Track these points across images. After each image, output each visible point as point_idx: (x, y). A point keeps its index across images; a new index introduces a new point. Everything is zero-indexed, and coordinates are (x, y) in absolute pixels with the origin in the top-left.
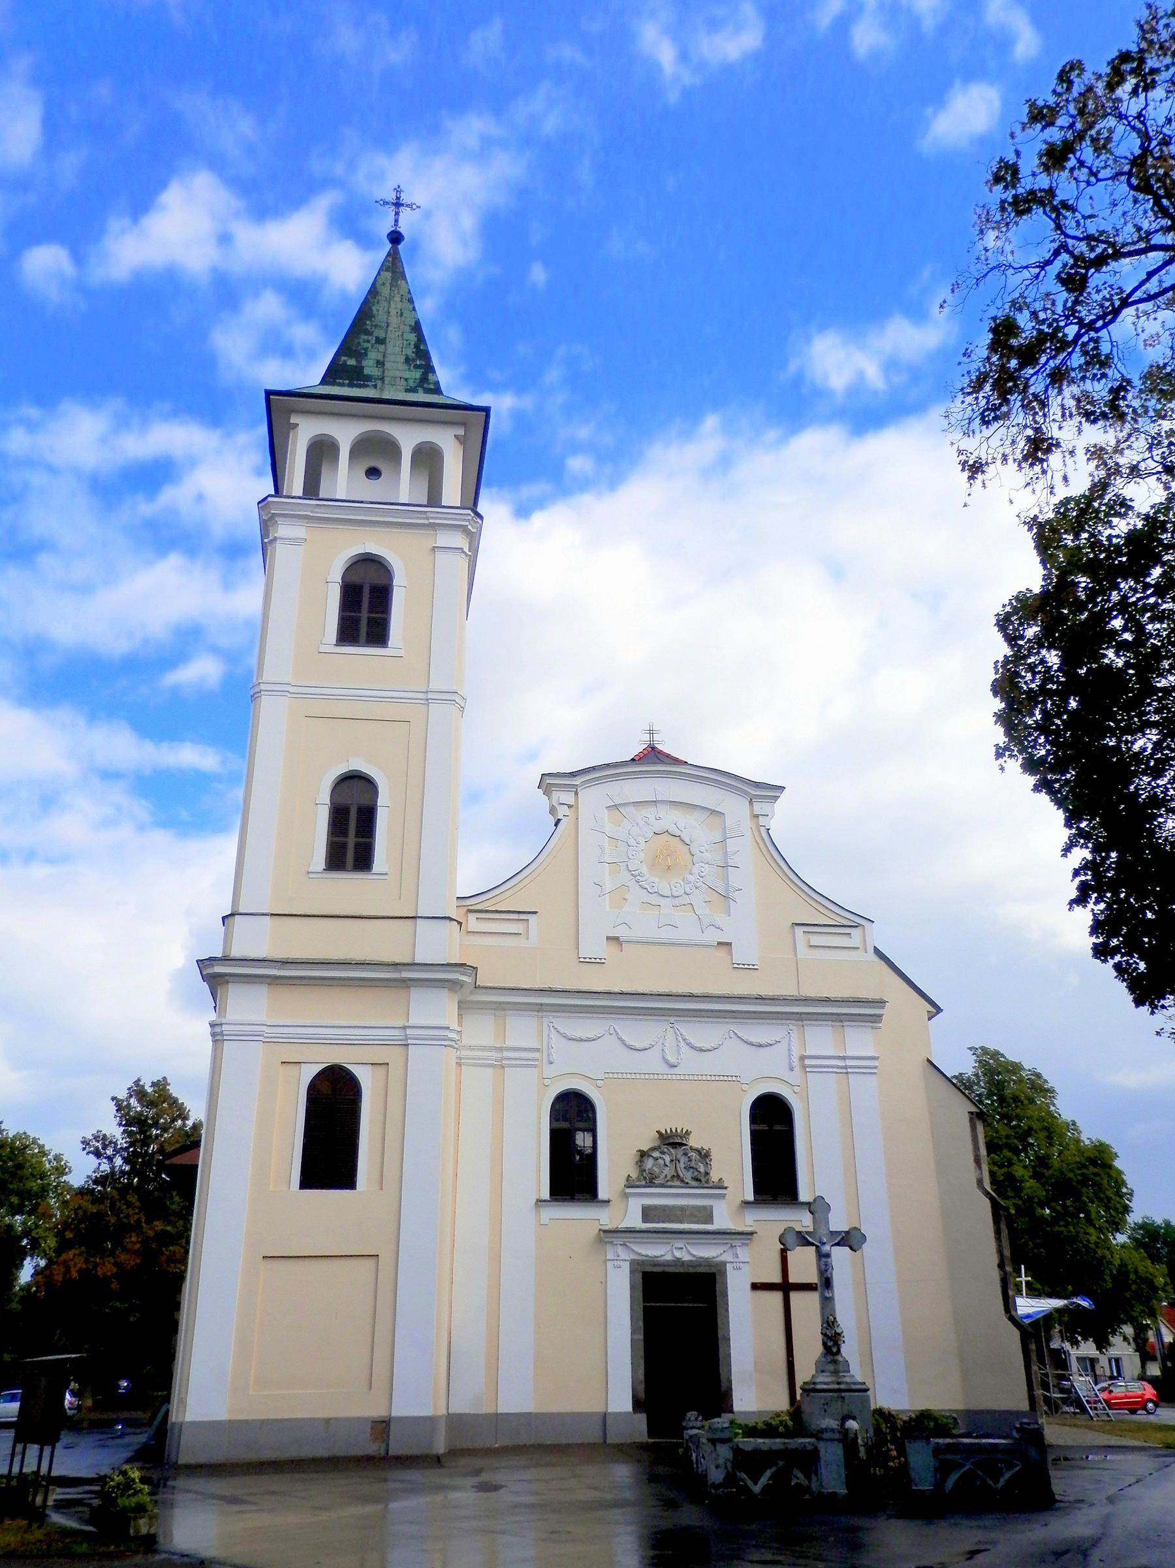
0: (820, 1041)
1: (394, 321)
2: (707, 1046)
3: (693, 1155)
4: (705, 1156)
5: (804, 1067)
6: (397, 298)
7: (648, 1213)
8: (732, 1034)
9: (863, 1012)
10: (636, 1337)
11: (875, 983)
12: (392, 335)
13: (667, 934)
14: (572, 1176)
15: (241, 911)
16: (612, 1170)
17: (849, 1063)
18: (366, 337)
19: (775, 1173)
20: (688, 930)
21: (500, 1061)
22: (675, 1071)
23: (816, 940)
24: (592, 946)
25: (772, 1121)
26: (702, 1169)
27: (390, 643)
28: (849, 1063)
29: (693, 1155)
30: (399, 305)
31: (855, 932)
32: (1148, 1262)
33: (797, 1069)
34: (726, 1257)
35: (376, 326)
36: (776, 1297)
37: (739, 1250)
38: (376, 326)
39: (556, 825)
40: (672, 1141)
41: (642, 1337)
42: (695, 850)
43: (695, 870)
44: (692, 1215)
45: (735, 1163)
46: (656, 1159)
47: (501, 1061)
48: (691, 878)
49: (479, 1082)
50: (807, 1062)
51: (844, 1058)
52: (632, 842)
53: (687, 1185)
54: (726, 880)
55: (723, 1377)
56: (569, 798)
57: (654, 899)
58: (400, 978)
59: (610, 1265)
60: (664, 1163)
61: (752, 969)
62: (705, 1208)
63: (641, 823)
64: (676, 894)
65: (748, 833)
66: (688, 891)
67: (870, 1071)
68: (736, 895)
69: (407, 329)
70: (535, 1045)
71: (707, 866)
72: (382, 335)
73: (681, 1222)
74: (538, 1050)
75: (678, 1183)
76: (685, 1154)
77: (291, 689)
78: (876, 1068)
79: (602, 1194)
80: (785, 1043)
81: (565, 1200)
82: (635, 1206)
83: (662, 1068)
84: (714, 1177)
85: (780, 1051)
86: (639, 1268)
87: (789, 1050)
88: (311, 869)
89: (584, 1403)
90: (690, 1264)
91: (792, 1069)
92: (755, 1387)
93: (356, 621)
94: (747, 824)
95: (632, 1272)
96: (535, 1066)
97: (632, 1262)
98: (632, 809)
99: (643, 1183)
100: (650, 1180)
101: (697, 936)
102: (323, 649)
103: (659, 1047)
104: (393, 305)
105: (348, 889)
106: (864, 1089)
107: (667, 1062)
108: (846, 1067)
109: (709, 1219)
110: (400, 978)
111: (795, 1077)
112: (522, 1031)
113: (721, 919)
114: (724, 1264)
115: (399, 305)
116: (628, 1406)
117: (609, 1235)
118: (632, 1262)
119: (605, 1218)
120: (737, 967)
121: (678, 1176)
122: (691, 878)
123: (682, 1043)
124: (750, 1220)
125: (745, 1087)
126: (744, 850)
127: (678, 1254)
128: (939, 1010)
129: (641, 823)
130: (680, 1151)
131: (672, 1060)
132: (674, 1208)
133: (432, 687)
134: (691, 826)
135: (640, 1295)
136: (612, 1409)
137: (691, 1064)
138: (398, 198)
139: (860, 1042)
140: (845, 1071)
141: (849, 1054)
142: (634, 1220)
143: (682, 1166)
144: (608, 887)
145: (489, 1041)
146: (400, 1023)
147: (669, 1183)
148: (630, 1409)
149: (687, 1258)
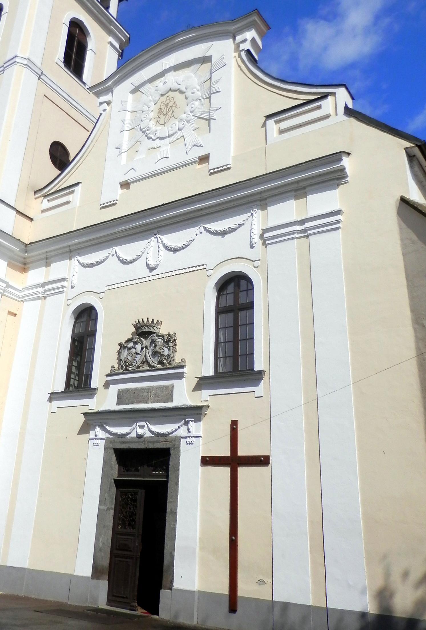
2: (179, 245)
4: (169, 340)
5: (264, 244)
7: (121, 397)
17: (308, 225)
22: (154, 272)
23: (285, 125)
26: (166, 352)
32: (153, 122)
34: (182, 432)
46: (130, 349)
52: (145, 108)
53: (153, 368)
62: (167, 387)
73: (147, 402)
76: (153, 342)
78: (338, 222)
79: (94, 384)
81: (420, 378)
84: (177, 359)
86: (111, 445)
90: (150, 440)
92: (193, 567)
95: (106, 449)
97: (107, 440)
98: (148, 86)
99: (121, 371)
106: (327, 247)
108: (305, 230)
117: (93, 420)
118: (107, 440)
119: (94, 404)
124: (204, 397)
125: (209, 273)
127: (140, 431)
132: (143, 389)
137: (168, 262)
147: (141, 369)
149: (148, 434)
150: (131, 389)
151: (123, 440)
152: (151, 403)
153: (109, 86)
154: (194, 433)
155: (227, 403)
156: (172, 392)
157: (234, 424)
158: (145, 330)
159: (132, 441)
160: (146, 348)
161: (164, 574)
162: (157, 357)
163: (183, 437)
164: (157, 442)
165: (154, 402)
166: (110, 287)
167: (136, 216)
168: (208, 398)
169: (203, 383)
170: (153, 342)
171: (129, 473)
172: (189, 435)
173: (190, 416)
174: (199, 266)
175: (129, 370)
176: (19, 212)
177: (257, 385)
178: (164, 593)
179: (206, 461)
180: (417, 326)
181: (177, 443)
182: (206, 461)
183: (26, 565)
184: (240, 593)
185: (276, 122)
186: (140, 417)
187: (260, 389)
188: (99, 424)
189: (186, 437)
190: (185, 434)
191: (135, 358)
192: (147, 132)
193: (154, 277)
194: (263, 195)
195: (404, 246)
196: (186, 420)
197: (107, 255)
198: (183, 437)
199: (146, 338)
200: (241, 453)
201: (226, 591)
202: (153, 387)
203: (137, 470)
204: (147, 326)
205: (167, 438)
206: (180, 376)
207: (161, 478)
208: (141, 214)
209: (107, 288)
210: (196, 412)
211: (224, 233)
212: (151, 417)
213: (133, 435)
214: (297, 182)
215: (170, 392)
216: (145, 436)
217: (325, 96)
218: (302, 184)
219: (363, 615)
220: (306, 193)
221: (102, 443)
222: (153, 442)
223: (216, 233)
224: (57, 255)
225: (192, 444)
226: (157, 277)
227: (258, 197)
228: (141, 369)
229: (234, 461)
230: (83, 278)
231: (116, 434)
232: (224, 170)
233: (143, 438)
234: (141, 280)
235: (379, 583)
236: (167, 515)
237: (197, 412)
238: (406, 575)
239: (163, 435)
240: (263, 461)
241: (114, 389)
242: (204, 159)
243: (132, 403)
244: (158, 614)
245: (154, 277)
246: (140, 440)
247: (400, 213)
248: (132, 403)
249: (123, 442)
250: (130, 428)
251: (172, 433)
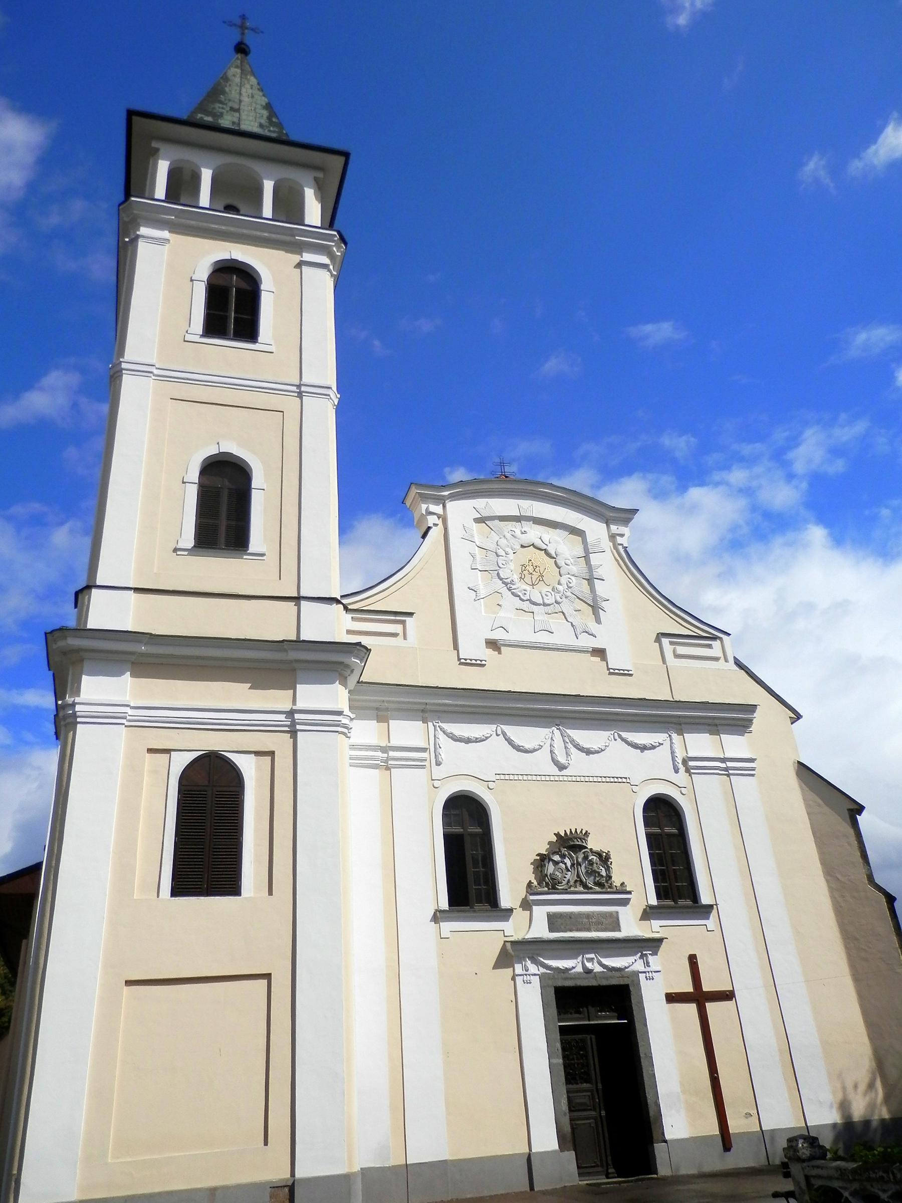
0: (700, 744)
1: (246, 100)
3: (594, 858)
5: (688, 770)
6: (248, 86)
7: (554, 922)
8: (617, 737)
9: (733, 719)
10: (554, 1061)
11: (741, 691)
12: (245, 107)
13: (543, 638)
14: (469, 880)
15: (98, 584)
16: (512, 875)
17: (730, 764)
18: (221, 106)
20: (562, 636)
21: (386, 760)
22: (564, 772)
23: (681, 650)
24: (472, 648)
25: (664, 821)
26: (604, 873)
27: (260, 339)
28: (730, 764)
29: (594, 858)
30: (250, 91)
31: (716, 644)
33: (682, 769)
34: (639, 966)
35: (230, 100)
36: (691, 1009)
37: (651, 959)
38: (230, 100)
39: (424, 536)
40: (570, 844)
42: (561, 563)
43: (564, 580)
45: (634, 869)
47: (386, 761)
48: (560, 588)
49: (361, 788)
50: (691, 763)
51: (723, 760)
52: (501, 552)
54: (593, 589)
55: (650, 1101)
56: (438, 509)
57: (526, 606)
58: (282, 663)
59: (519, 980)
60: (563, 869)
61: (627, 674)
62: (610, 914)
63: (508, 535)
64: (547, 602)
65: (608, 550)
66: (559, 600)
67: (749, 773)
68: (604, 604)
69: (259, 107)
70: (422, 744)
71: (573, 578)
72: (236, 106)
74: (424, 750)
75: (581, 889)
76: (586, 858)
77: (156, 372)
78: (753, 769)
82: (540, 913)
83: (555, 770)
84: (616, 880)
85: (663, 753)
86: (550, 982)
87: (673, 753)
88: (180, 546)
89: (506, 1143)
91: (677, 771)
92: (681, 1117)
93: (225, 319)
94: (607, 545)
96: (423, 767)
100: (553, 885)
101: (572, 642)
102: (189, 337)
103: (546, 749)
104: (244, 90)
105: (219, 570)
108: (726, 769)
109: (617, 927)
110: (282, 663)
111: (682, 778)
112: (408, 732)
113: (592, 626)
114: (636, 974)
115: (250, 91)
116: (554, 1145)
118: (542, 977)
120: (612, 673)
121: (581, 881)
122: (560, 588)
123: (570, 746)
124: (655, 928)
126: (606, 563)
128: (799, 717)
129: (508, 535)
130: (581, 856)
131: (562, 759)
132: (580, 915)
133: (304, 380)
134: (557, 541)
136: (538, 1147)
138: (243, 23)
139: (734, 745)
140: (727, 772)
141: (728, 755)
142: (540, 930)
144: (483, 592)
145: (374, 741)
146: (288, 707)
147: (572, 889)
148: (556, 1147)
149: (598, 969)
151: (566, 975)
153: (444, 496)
154: (653, 967)
155: (680, 935)
161: (653, 1127)
164: (611, 977)
166: (502, 777)
167: (562, 698)
168: (659, 929)
169: (649, 913)
170: (586, 858)
171: (566, 1016)
173: (648, 949)
176: (137, 590)
177: (708, 918)
178: (659, 1148)
179: (672, 998)
180: (829, 878)
182: (672, 998)
183: (445, 1155)
185: (671, 643)
187: (711, 923)
189: (644, 972)
190: (642, 969)
192: (513, 587)
195: (807, 806)
200: (706, 988)
201: (713, 1129)
202: (593, 912)
203: (579, 1013)
206: (625, 903)
208: (548, 697)
210: (648, 946)
211: (643, 748)
212: (602, 949)
214: (714, 718)
217: (715, 638)
219: (835, 1125)
222: (607, 978)
223: (635, 746)
224: (399, 710)
228: (572, 889)
229: (699, 997)
230: (478, 759)
231: (558, 969)
232: (625, 675)
235: (840, 1096)
236: (642, 1060)
237: (655, 944)
238: (856, 1087)
240: (728, 996)
241: (540, 913)
242: (600, 653)
243: (571, 931)
247: (798, 774)
249: (566, 979)
251: (570, 969)
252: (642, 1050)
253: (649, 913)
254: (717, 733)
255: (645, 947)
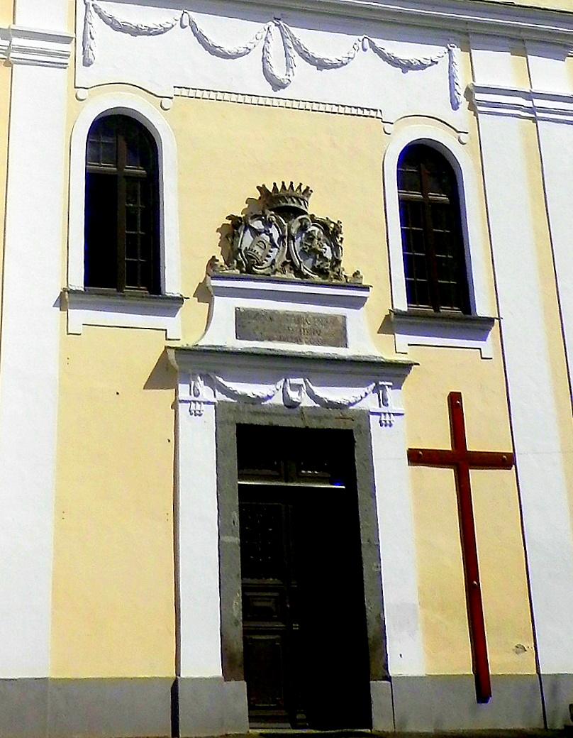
2: (333, 58)
3: (316, 231)
5: (472, 107)
7: (245, 323)
14: (120, 252)
16: (186, 245)
17: (538, 103)
19: (439, 279)
25: (430, 186)
28: (538, 103)
33: (464, 103)
34: (371, 403)
36: (445, 477)
41: (237, 540)
44: (315, 332)
45: (375, 250)
50: (478, 96)
51: (529, 96)
60: (263, 242)
62: (333, 320)
70: (66, 31)
74: (67, 40)
76: (303, 228)
79: (172, 286)
80: (444, 63)
82: (225, 308)
83: (267, 89)
86: (231, 417)
91: (455, 106)
92: (416, 643)
100: (249, 268)
103: (256, 55)
107: (270, 77)
108: (532, 110)
111: (462, 117)
114: (366, 415)
118: (219, 407)
119: (185, 328)
121: (292, 264)
124: (400, 347)
132: (287, 316)
135: (233, 462)
140: (533, 115)
142: (223, 334)
143: (298, 248)
147: (278, 275)
150: (264, 311)
151: (256, 408)
152: (307, 343)
154: (393, 407)
155: (439, 360)
156: (345, 328)
157: (455, 401)
158: (292, 205)
159: (274, 410)
160: (291, 237)
162: (311, 260)
163: (373, 413)
165: (312, 344)
169: (394, 322)
170: (303, 228)
172: (384, 409)
173: (388, 377)
174: (368, 109)
175: (255, 273)
178: (378, 688)
179: (418, 457)
181: (364, 423)
182: (418, 457)
183: (44, 669)
184: (542, 673)
186: (296, 370)
187: (488, 346)
188: (204, 372)
191: (270, 254)
193: (276, 102)
194: (468, 27)
196: (381, 383)
197: (172, 21)
198: (373, 413)
199: (287, 219)
201: (465, 667)
202: (307, 314)
204: (297, 198)
205: (345, 412)
206: (357, 303)
207: (324, 483)
209: (178, 91)
210: (397, 371)
211: (407, 66)
213: (278, 400)
215: (341, 328)
216: (301, 405)
218: (523, 35)
220: (469, 43)
221: (209, 412)
222: (320, 418)
225: (391, 425)
226: (282, 103)
227: (514, 34)
228: (278, 275)
231: (245, 396)
233: (298, 409)
234: (255, 100)
237: (398, 372)
239: (339, 406)
240: (504, 461)
241: (225, 308)
244: (371, 727)
245: (276, 102)
246: (291, 410)
248: (270, 340)
249: (256, 413)
250: (272, 387)
252: (364, 533)
253: (394, 322)
254: (524, 53)
255: (383, 374)
